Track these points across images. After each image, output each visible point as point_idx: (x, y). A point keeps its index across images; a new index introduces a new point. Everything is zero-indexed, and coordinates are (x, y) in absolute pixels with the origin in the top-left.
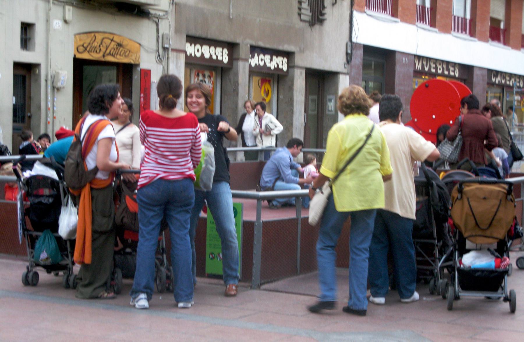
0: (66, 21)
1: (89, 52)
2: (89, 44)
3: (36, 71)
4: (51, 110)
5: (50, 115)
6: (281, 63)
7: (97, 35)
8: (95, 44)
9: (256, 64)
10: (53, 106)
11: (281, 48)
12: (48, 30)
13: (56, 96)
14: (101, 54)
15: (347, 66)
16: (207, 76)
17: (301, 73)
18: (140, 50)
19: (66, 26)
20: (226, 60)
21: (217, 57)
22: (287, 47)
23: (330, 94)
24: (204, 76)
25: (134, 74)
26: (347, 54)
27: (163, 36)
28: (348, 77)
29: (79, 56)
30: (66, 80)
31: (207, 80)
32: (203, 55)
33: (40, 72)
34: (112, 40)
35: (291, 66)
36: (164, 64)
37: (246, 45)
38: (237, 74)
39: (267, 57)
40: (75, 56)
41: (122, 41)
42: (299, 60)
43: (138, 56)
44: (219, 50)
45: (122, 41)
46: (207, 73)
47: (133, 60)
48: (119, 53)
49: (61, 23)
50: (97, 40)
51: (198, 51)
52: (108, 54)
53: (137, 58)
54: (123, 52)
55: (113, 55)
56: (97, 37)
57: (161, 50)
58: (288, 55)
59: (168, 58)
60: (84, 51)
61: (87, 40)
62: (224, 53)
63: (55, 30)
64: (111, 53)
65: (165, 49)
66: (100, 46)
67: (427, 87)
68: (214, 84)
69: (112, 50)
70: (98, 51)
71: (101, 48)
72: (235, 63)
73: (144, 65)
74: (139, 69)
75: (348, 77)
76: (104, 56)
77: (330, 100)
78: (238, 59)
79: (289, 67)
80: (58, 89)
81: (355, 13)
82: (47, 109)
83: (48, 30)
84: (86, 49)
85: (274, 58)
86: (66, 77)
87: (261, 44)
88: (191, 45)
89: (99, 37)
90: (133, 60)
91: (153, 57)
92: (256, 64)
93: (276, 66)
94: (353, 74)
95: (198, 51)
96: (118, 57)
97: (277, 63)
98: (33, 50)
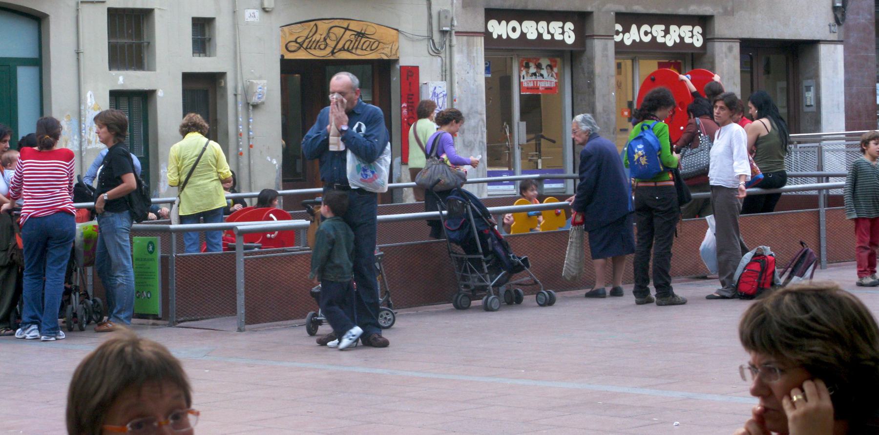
0: (265, 10)
1: (306, 49)
2: (307, 38)
3: (221, 82)
4: (245, 136)
5: (243, 142)
6: (693, 36)
7: (319, 23)
8: (317, 37)
9: (634, 41)
10: (249, 130)
11: (681, 11)
12: (235, 26)
13: (251, 116)
14: (329, 50)
15: (836, 28)
16: (544, 66)
17: (730, 49)
18: (397, 40)
19: (266, 15)
21: (552, 35)
22: (694, 9)
23: (808, 78)
24: (539, 66)
25: (392, 74)
26: (835, 8)
27: (439, 13)
28: (840, 48)
29: (289, 56)
30: (265, 92)
31: (544, 72)
32: (523, 35)
33: (226, 83)
34: (347, 29)
35: (708, 39)
36: (443, 55)
37: (608, 12)
38: (591, 60)
39: (658, 30)
40: (282, 56)
41: (364, 28)
42: (720, 28)
43: (395, 48)
44: (555, 26)
45: (364, 28)
46: (545, 62)
47: (386, 55)
48: (360, 46)
49: (257, 13)
50: (319, 32)
51: (514, 30)
52: (340, 50)
53: (394, 52)
54: (367, 43)
55: (348, 50)
56: (319, 27)
57: (437, 37)
58: (704, 21)
59: (451, 46)
60: (299, 48)
61: (302, 32)
62: (566, 29)
63: (248, 23)
64: (346, 47)
65: (444, 33)
66: (325, 39)
67: (653, 80)
68: (560, 77)
69: (348, 43)
70: (322, 47)
71: (328, 41)
72: (588, 42)
73: (405, 61)
74: (398, 67)
75: (840, 48)
76: (333, 53)
77: (808, 89)
78: (592, 37)
79: (706, 40)
80: (255, 106)
82: (239, 135)
83: (235, 26)
84: (301, 45)
85: (673, 28)
86: (266, 88)
87: (638, 9)
88: (500, 23)
89: (323, 27)
90: (386, 55)
91: (423, 47)
92: (634, 41)
93: (678, 41)
94: (851, 41)
95: (514, 30)
96: (359, 52)
97: (679, 36)
98: (215, 55)
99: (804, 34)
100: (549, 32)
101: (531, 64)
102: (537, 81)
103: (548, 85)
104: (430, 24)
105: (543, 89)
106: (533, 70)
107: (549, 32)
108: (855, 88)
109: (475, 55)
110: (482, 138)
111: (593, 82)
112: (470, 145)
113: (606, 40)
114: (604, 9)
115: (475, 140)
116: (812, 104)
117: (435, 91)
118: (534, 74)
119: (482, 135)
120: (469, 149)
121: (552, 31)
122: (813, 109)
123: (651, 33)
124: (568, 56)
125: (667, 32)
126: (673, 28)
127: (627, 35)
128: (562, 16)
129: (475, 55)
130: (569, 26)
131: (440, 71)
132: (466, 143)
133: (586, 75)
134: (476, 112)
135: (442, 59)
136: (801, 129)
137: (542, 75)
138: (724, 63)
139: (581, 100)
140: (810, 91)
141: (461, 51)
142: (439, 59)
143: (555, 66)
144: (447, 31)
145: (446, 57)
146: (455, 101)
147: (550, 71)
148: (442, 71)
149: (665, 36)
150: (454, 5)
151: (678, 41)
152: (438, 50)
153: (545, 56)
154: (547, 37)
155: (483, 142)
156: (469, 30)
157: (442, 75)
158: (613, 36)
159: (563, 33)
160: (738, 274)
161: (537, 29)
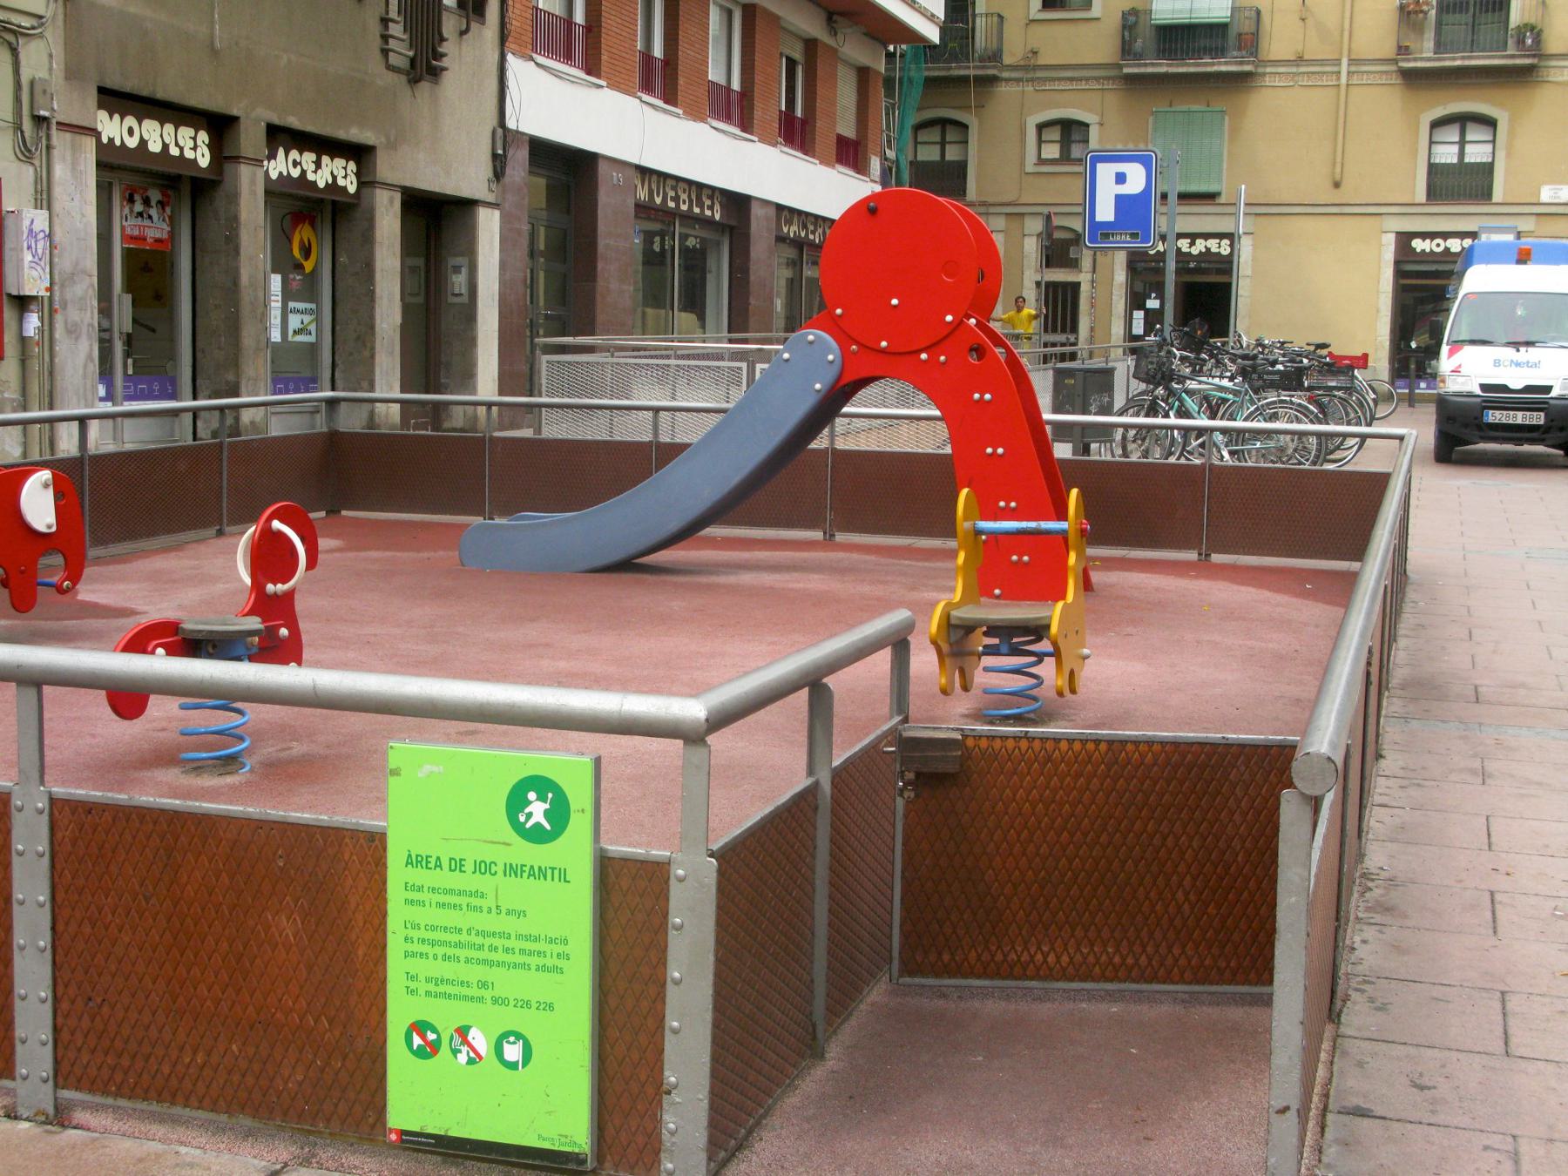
11: (342, 134)
15: (494, 186)
16: (153, 203)
17: (391, 201)
21: (181, 149)
22: (355, 134)
23: (456, 255)
24: (147, 202)
26: (495, 156)
27: (32, 83)
31: (153, 212)
32: (143, 143)
35: (366, 181)
42: (387, 168)
57: (27, 125)
58: (359, 153)
59: (49, 147)
65: (39, 121)
68: (173, 221)
77: (457, 270)
78: (236, 159)
79: (361, 184)
81: (510, 57)
85: (325, 159)
87: (293, 122)
95: (131, 132)
99: (465, 192)
100: (177, 144)
101: (137, 197)
102: (144, 226)
103: (158, 235)
104: (18, 100)
105: (152, 240)
106: (139, 207)
107: (177, 144)
108: (508, 274)
109: (82, 168)
110: (92, 318)
111: (237, 236)
112: (75, 331)
113: (255, 168)
114: (253, 115)
115: (82, 321)
116: (463, 291)
117: (33, 226)
118: (140, 214)
119: (92, 313)
120: (73, 336)
121: (181, 143)
122: (465, 299)
123: (300, 164)
124: (186, 189)
125: (1192, 244)
126: (1198, 241)
127: (1193, 248)
128: (1220, 236)
129: (82, 168)
131: (33, 191)
132: (69, 326)
133: (223, 222)
134: (84, 272)
135: (36, 169)
136: (600, 318)
137: (150, 217)
138: (385, 222)
139: (211, 263)
140: (460, 273)
141: (64, 159)
142: (31, 169)
143: (168, 204)
144: (45, 119)
145: (41, 167)
146: (56, 248)
147: (161, 211)
148: (36, 192)
149: (315, 172)
150: (54, 73)
151: (1204, 250)
152: (29, 151)
153: (155, 185)
154: (174, 151)
155: (93, 326)
156: (75, 123)
157: (36, 199)
158: (262, 161)
159: (1219, 247)
160: (1105, 579)
161: (161, 136)
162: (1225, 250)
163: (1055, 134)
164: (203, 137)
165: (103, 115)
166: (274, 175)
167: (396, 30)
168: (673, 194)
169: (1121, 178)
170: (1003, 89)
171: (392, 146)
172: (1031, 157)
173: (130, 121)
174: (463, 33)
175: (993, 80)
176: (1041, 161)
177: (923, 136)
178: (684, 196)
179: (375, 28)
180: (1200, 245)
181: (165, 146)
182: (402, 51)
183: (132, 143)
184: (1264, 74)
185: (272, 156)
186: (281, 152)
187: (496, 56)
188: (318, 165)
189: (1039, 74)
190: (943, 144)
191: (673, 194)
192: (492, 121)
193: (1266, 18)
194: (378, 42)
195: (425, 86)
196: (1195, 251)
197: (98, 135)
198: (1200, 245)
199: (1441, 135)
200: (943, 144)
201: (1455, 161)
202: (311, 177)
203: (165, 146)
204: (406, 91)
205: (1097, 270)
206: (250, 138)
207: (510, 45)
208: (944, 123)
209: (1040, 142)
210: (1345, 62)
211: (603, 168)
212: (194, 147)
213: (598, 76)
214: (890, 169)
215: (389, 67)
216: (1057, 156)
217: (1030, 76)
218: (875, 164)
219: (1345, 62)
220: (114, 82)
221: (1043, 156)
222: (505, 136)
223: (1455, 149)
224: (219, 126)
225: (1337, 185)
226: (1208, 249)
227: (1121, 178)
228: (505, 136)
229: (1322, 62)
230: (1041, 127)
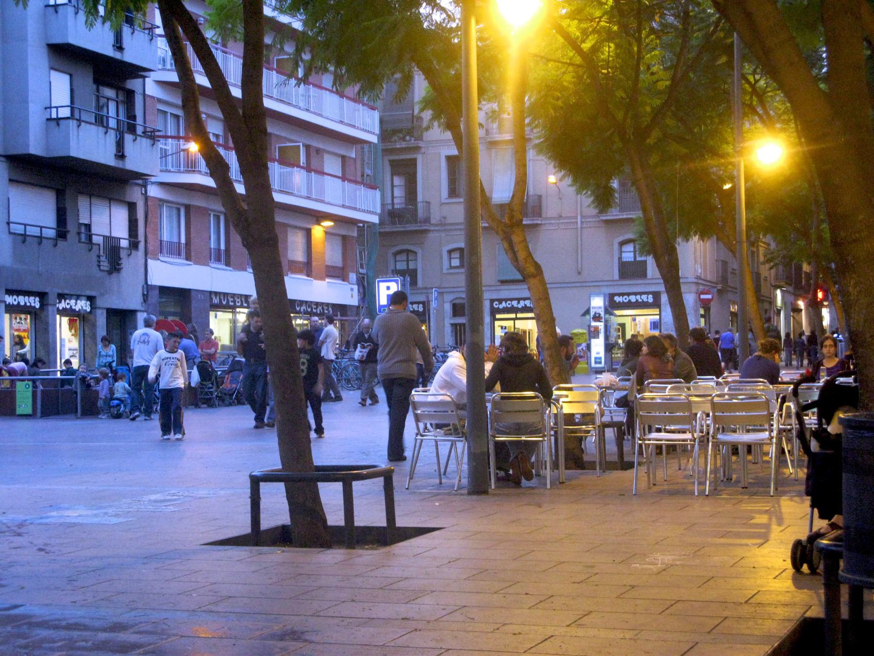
15: (144, 305)
17: (102, 313)
20: (38, 306)
26: (144, 295)
32: (19, 303)
81: (149, 261)
95: (15, 300)
106: (18, 320)
125: (519, 303)
126: (521, 302)
130: (650, 296)
154: (28, 304)
162: (421, 309)
163: (456, 255)
164: (37, 299)
165: (7, 296)
166: (61, 308)
167: (103, 259)
168: (232, 299)
169: (388, 288)
170: (431, 235)
171: (102, 295)
172: (446, 264)
173: (15, 297)
174: (129, 255)
175: (426, 231)
176: (451, 267)
177: (398, 258)
178: (237, 300)
179: (95, 259)
180: (522, 303)
181: (25, 303)
182: (105, 265)
183: (16, 303)
184: (545, 224)
185: (60, 302)
186: (63, 301)
187: (143, 261)
188: (76, 304)
189: (449, 227)
190: (408, 261)
191: (232, 299)
192: (143, 283)
193: (544, 198)
194: (97, 263)
195: (115, 275)
196: (520, 306)
197: (5, 302)
198: (504, 305)
199: (625, 248)
200: (408, 261)
201: (633, 260)
202: (73, 308)
203: (25, 303)
204: (108, 277)
205: (7, 200)
206: (52, 298)
207: (148, 256)
208: (408, 251)
209: (450, 259)
210: (579, 217)
211: (193, 293)
212: (34, 302)
213: (190, 261)
214: (363, 278)
215: (100, 270)
216: (458, 264)
217: (443, 228)
218: (353, 277)
219: (579, 217)
220: (10, 287)
221: (452, 265)
222: (148, 288)
223: (632, 255)
224: (42, 296)
225: (579, 273)
226: (525, 305)
227: (388, 288)
228: (147, 288)
229: (569, 218)
230: (450, 252)
